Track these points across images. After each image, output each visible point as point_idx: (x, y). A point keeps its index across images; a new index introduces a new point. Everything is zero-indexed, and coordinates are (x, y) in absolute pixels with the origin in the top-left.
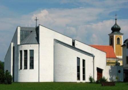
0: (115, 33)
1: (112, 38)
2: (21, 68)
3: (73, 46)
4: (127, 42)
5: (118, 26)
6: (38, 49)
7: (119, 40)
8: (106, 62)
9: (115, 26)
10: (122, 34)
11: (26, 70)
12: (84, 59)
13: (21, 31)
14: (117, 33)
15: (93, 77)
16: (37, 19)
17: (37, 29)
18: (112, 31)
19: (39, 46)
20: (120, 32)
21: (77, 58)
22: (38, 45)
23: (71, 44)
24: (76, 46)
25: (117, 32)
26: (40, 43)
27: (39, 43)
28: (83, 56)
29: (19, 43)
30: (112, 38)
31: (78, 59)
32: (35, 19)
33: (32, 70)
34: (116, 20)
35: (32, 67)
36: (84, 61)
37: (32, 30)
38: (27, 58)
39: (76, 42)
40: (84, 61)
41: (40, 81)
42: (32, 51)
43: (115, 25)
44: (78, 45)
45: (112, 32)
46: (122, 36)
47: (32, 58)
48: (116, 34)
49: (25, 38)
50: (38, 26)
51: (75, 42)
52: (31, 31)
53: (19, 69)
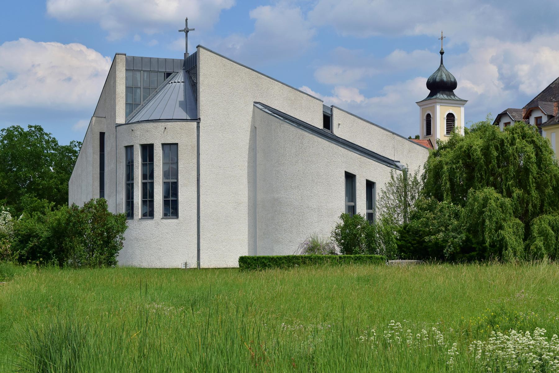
0: (439, 96)
1: (429, 116)
3: (327, 130)
4: (505, 120)
5: (448, 75)
6: (195, 161)
7: (453, 121)
8: (68, 203)
9: (439, 75)
10: (462, 102)
11: (148, 223)
12: (370, 179)
13: (131, 73)
14: (445, 97)
16: (189, 27)
18: (429, 92)
19: (198, 127)
20: (454, 95)
22: (195, 124)
23: (319, 124)
24: (337, 131)
25: (447, 95)
26: (202, 115)
27: (197, 119)
28: (392, 169)
29: (121, 119)
30: (429, 116)
31: (350, 178)
32: (183, 27)
33: (172, 222)
34: (442, 53)
36: (370, 185)
37: (168, 71)
38: (152, 176)
39: (337, 118)
40: (370, 185)
41: (203, 265)
43: (439, 70)
45: (431, 95)
46: (462, 109)
48: (443, 102)
50: (191, 51)
51: (332, 115)
52: (168, 75)
53: (140, 217)
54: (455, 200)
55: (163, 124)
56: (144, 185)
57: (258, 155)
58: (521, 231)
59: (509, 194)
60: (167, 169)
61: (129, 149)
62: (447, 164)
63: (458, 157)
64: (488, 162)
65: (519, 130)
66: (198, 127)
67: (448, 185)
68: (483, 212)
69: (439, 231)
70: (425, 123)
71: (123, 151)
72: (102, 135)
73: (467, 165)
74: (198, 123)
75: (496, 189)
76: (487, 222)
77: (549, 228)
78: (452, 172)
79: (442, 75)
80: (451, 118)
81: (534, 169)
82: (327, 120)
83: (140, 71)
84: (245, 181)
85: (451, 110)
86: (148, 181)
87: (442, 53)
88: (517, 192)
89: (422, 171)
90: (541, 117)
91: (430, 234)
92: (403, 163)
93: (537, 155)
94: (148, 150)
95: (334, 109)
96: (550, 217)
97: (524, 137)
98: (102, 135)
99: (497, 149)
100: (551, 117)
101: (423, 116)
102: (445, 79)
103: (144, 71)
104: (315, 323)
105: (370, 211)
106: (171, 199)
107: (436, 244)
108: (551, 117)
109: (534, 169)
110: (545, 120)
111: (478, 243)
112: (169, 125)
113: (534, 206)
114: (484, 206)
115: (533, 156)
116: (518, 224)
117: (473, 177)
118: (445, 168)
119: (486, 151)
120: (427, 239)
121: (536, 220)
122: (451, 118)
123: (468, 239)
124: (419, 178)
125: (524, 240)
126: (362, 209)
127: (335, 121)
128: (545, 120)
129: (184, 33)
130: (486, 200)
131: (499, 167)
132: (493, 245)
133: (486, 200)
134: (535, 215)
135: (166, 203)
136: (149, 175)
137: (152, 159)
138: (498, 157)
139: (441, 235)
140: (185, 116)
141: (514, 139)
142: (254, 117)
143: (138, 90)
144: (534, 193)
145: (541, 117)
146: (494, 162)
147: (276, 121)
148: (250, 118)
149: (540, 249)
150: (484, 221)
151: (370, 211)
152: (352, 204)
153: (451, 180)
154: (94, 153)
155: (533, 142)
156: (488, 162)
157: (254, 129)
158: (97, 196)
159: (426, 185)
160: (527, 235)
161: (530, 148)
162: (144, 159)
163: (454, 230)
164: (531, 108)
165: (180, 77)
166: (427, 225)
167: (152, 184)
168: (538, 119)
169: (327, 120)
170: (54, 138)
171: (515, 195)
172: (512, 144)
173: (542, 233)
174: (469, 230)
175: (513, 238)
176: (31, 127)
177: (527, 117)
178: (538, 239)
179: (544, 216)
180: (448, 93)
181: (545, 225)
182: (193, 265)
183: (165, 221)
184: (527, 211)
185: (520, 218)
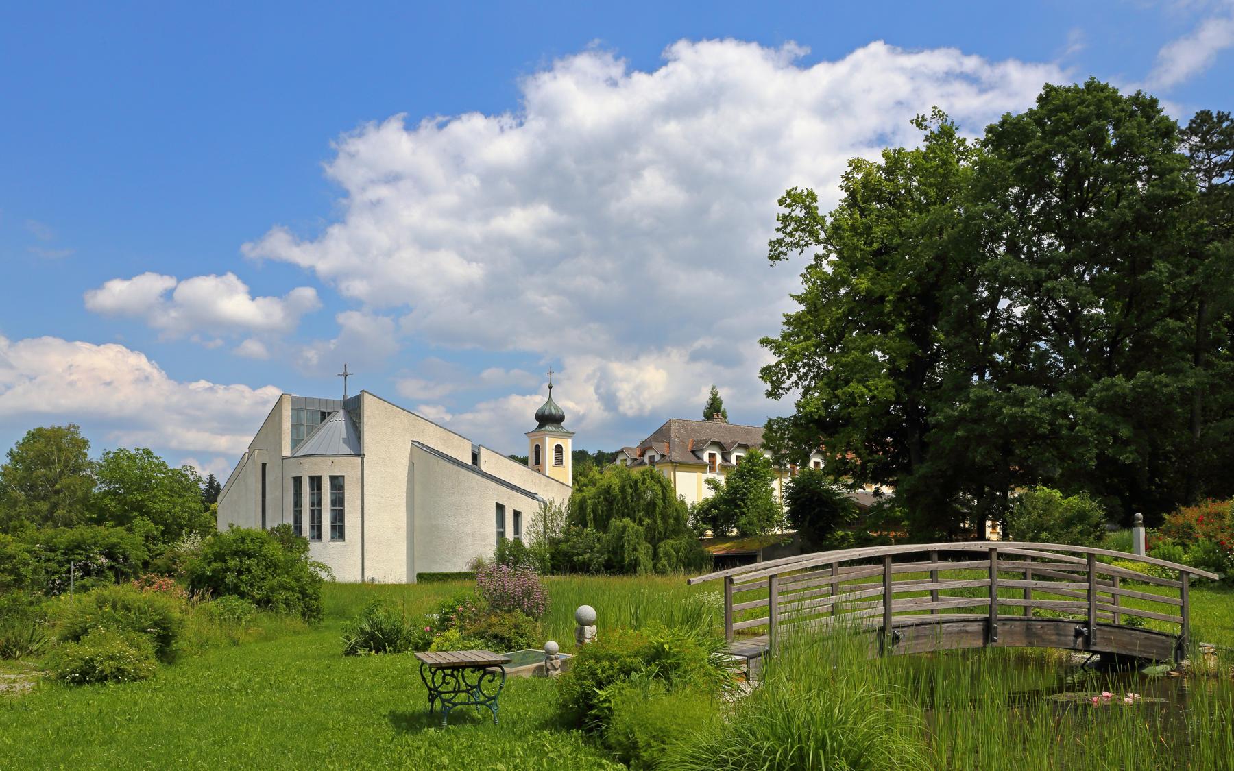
1: (537, 447)
2: (318, 536)
3: (474, 466)
5: (557, 408)
10: (569, 435)
12: (517, 509)
14: (554, 429)
15: (222, 487)
16: (348, 372)
17: (353, 409)
19: (363, 462)
20: (562, 428)
21: (515, 511)
23: (469, 461)
24: (484, 467)
27: (360, 454)
29: (287, 452)
30: (537, 447)
31: (500, 508)
33: (339, 544)
34: (550, 387)
35: (339, 532)
36: (517, 514)
38: (320, 504)
39: (484, 455)
40: (517, 514)
42: (338, 483)
43: (547, 403)
44: (489, 462)
45: (540, 427)
46: (570, 441)
47: (338, 501)
48: (552, 435)
49: (308, 433)
51: (479, 453)
54: (597, 528)
55: (332, 459)
56: (312, 512)
57: (416, 487)
58: (651, 552)
59: (640, 524)
60: (334, 498)
61: (298, 481)
62: (590, 498)
63: (600, 494)
64: (624, 498)
65: (648, 473)
66: (363, 462)
67: (592, 516)
68: (623, 537)
69: (585, 553)
70: (534, 453)
71: (291, 482)
72: (264, 465)
73: (606, 500)
74: (363, 458)
75: (631, 519)
76: (626, 545)
77: (672, 551)
78: (595, 505)
79: (550, 409)
80: (559, 449)
81: (660, 503)
82: (475, 457)
83: (303, 410)
84: (403, 509)
85: (559, 442)
86: (316, 508)
87: (550, 387)
88: (647, 521)
89: (566, 504)
90: (654, 456)
91: (578, 554)
92: (541, 495)
93: (662, 492)
94: (316, 481)
95: (481, 448)
96: (672, 542)
97: (652, 478)
98: (264, 465)
99: (631, 487)
100: (663, 456)
101: (532, 447)
102: (553, 412)
103: (308, 410)
104: (225, 729)
105: (517, 536)
106: (337, 524)
107: (584, 562)
108: (663, 456)
109: (660, 503)
110: (657, 458)
111: (617, 562)
112: (336, 459)
113: (660, 533)
114: (623, 532)
115: (660, 493)
116: (648, 548)
117: (612, 509)
118: (589, 502)
119: (623, 489)
120: (575, 558)
121: (661, 544)
122: (559, 449)
123: (609, 559)
124: (563, 509)
125: (653, 560)
126: (510, 535)
127: (482, 458)
128: (657, 458)
129: (343, 377)
130: (624, 528)
131: (632, 501)
132: (630, 564)
133: (624, 528)
134: (660, 540)
135: (333, 528)
136: (317, 503)
137: (320, 489)
138: (632, 494)
139: (587, 556)
140: (349, 451)
141: (644, 480)
142: (411, 454)
143: (302, 428)
144: (659, 522)
145: (654, 456)
146: (629, 498)
147: (433, 459)
148: (408, 454)
149: (665, 566)
150: (623, 545)
151: (517, 536)
152: (502, 530)
153: (593, 511)
154: (256, 482)
155: (659, 482)
156: (624, 498)
157: (412, 465)
158: (290, 521)
159: (570, 515)
160: (655, 556)
161: (657, 487)
162: (312, 489)
163: (598, 552)
164: (644, 448)
165: (340, 416)
166: (574, 547)
167: (320, 512)
168: (652, 458)
169: (475, 457)
170: (164, 462)
171: (645, 523)
172: (643, 484)
173: (667, 555)
174: (609, 552)
175: (645, 558)
176: (138, 449)
177: (642, 455)
178: (663, 559)
179: (668, 541)
180: (556, 425)
181: (668, 548)
182: (359, 579)
183: (333, 544)
184: (654, 536)
185: (649, 543)
